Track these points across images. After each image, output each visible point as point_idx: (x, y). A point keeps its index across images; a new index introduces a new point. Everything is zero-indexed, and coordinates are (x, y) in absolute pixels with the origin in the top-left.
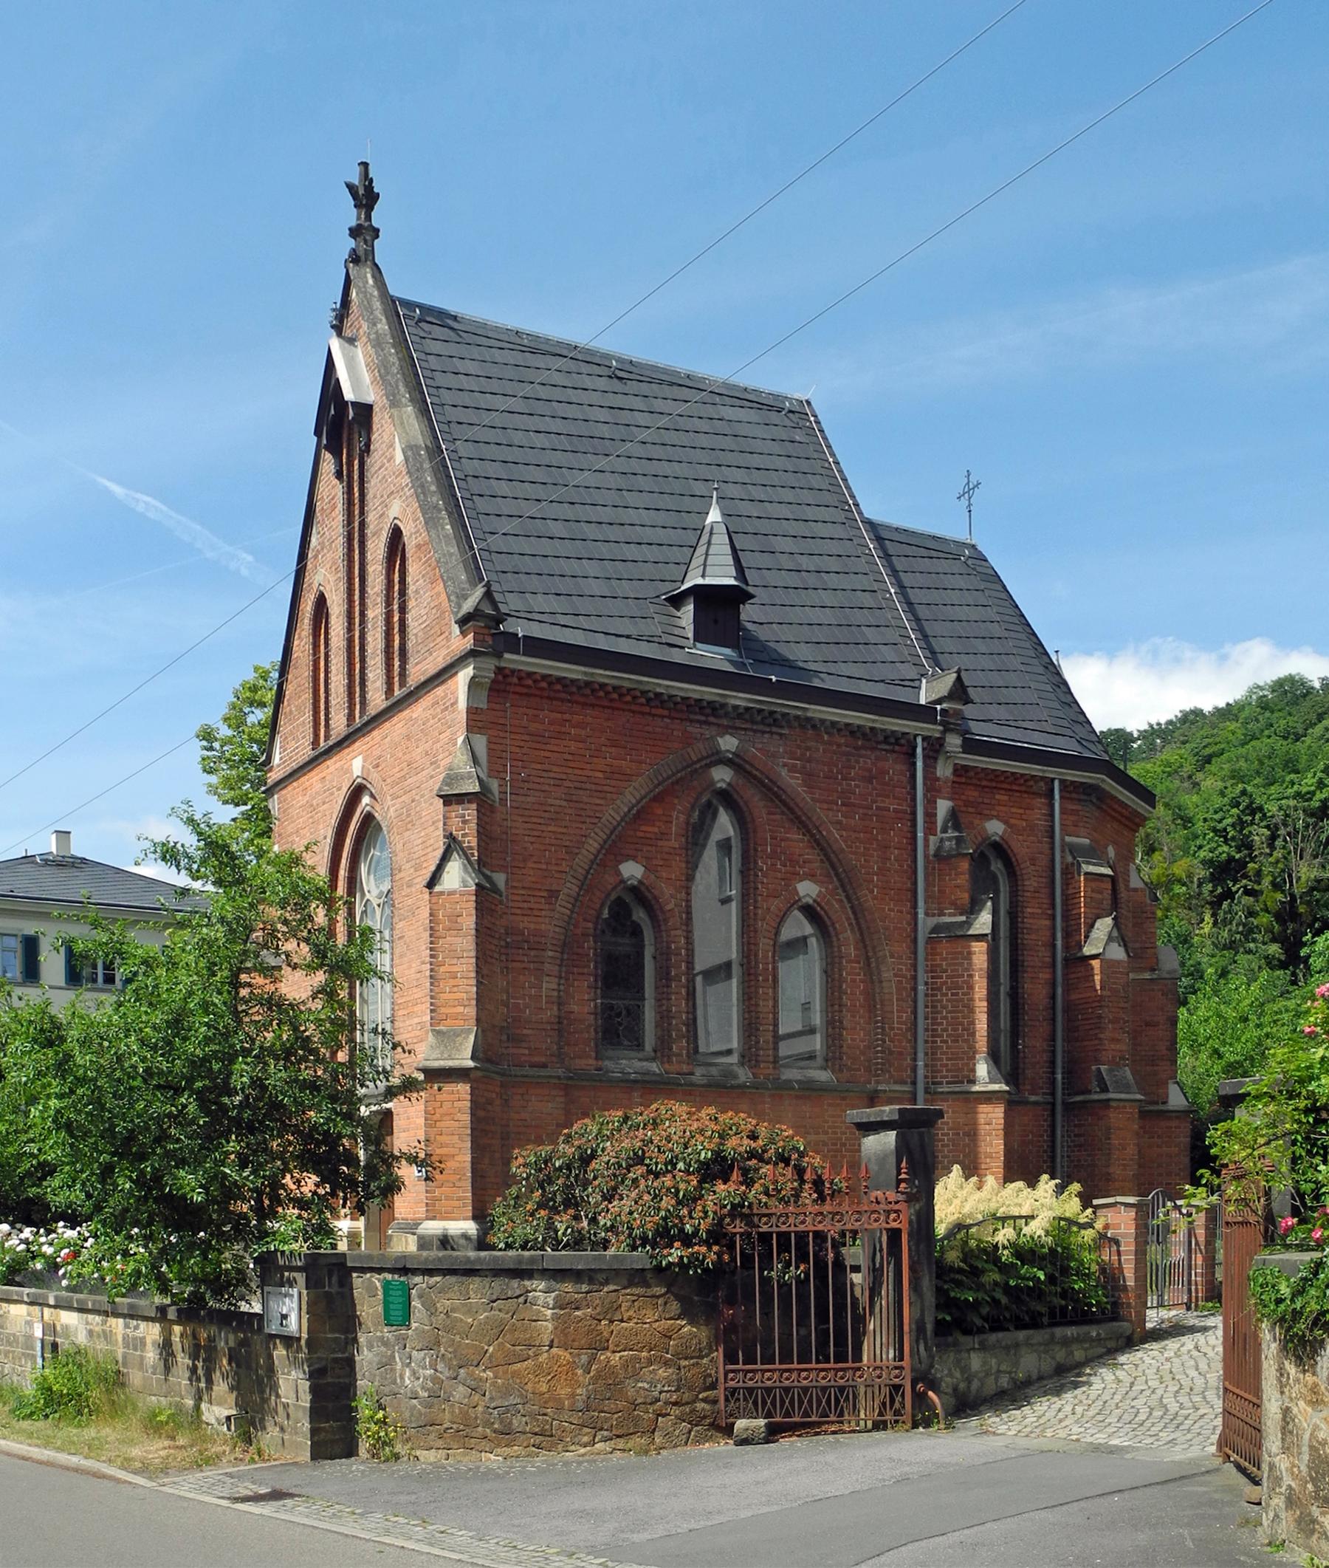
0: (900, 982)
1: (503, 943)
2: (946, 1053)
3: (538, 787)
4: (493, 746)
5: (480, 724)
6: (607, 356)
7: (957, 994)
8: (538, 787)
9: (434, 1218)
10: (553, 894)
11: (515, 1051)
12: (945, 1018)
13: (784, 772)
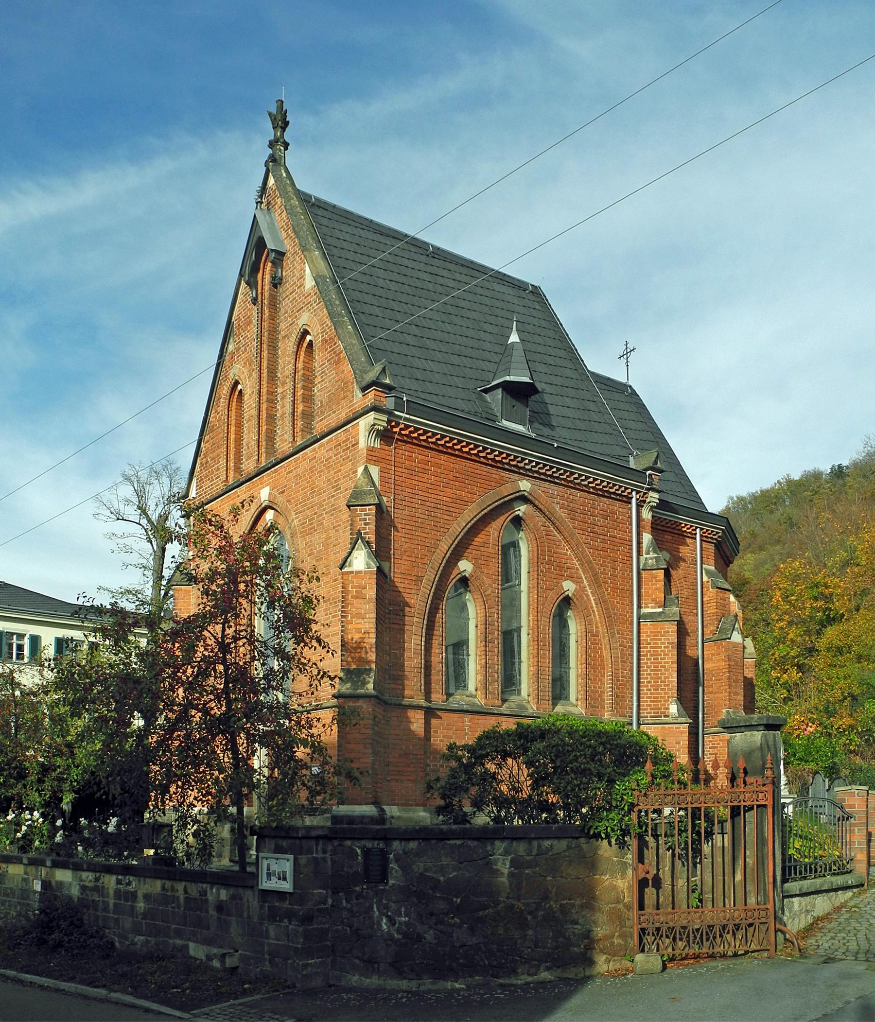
0: (623, 650)
1: (387, 611)
2: (650, 698)
3: (410, 504)
4: (384, 474)
5: (374, 458)
6: (427, 244)
7: (657, 659)
8: (410, 504)
9: (343, 804)
10: (419, 579)
11: (393, 686)
12: (650, 674)
13: (557, 508)
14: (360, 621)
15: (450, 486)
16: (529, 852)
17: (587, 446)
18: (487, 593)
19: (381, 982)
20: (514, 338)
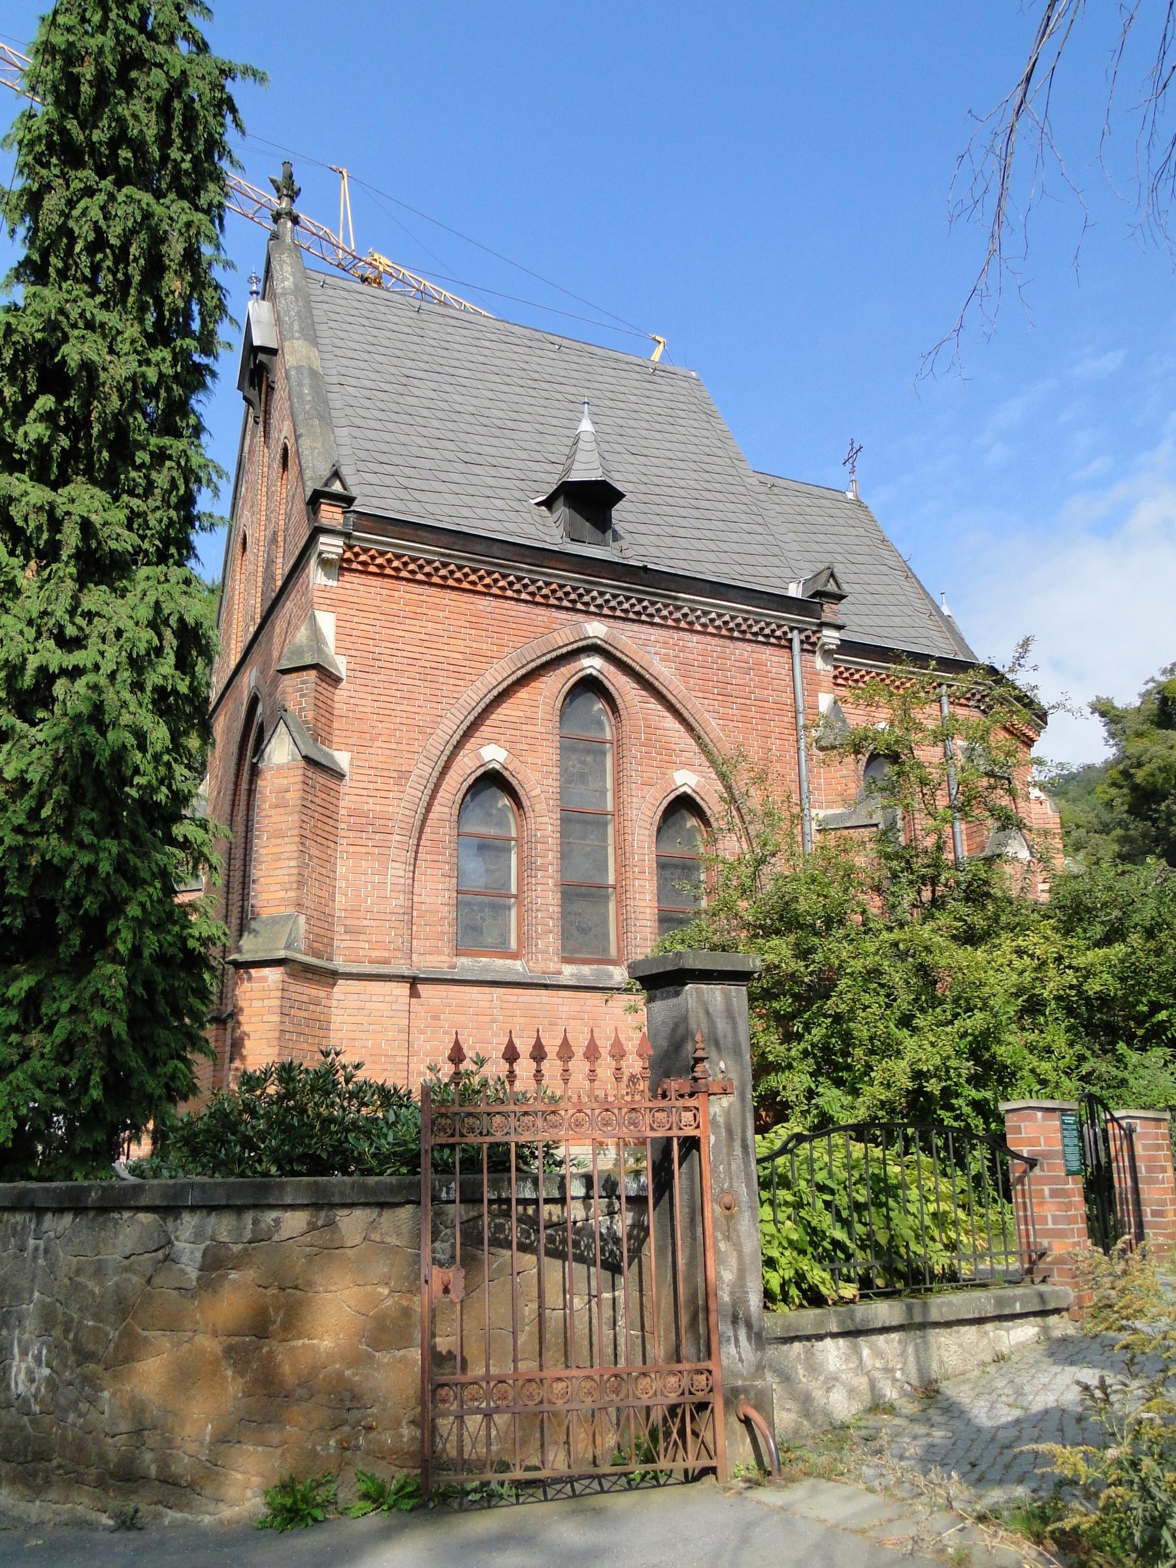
13: (656, 660)
14: (280, 841)
15: (461, 636)
16: (237, 1233)
17: (415, 507)
18: (534, 793)
19: (23, 1505)
20: (586, 426)
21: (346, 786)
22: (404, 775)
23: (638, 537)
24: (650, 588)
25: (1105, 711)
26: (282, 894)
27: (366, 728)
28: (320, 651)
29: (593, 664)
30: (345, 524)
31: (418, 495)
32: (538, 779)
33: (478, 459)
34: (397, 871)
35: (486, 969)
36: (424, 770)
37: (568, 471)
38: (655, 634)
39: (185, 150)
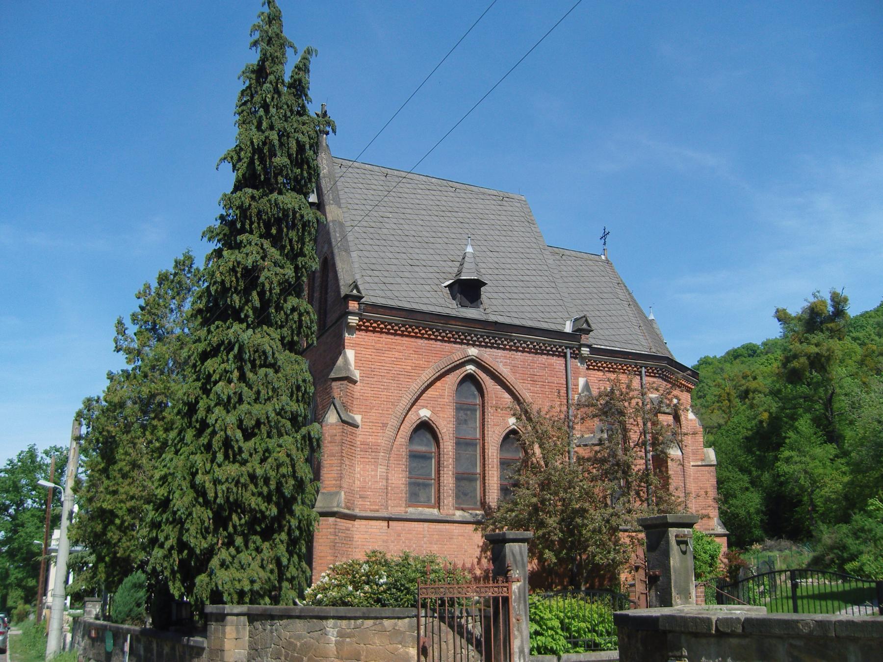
13: (501, 365)
21: (359, 431)
22: (385, 425)
23: (494, 306)
24: (498, 334)
25: (782, 317)
26: (334, 482)
27: (368, 403)
28: (349, 370)
29: (470, 368)
30: (359, 309)
31: (390, 287)
32: (446, 427)
33: (417, 263)
34: (381, 470)
35: (421, 514)
36: (393, 422)
37: (459, 273)
38: (500, 353)
39: (304, 174)
